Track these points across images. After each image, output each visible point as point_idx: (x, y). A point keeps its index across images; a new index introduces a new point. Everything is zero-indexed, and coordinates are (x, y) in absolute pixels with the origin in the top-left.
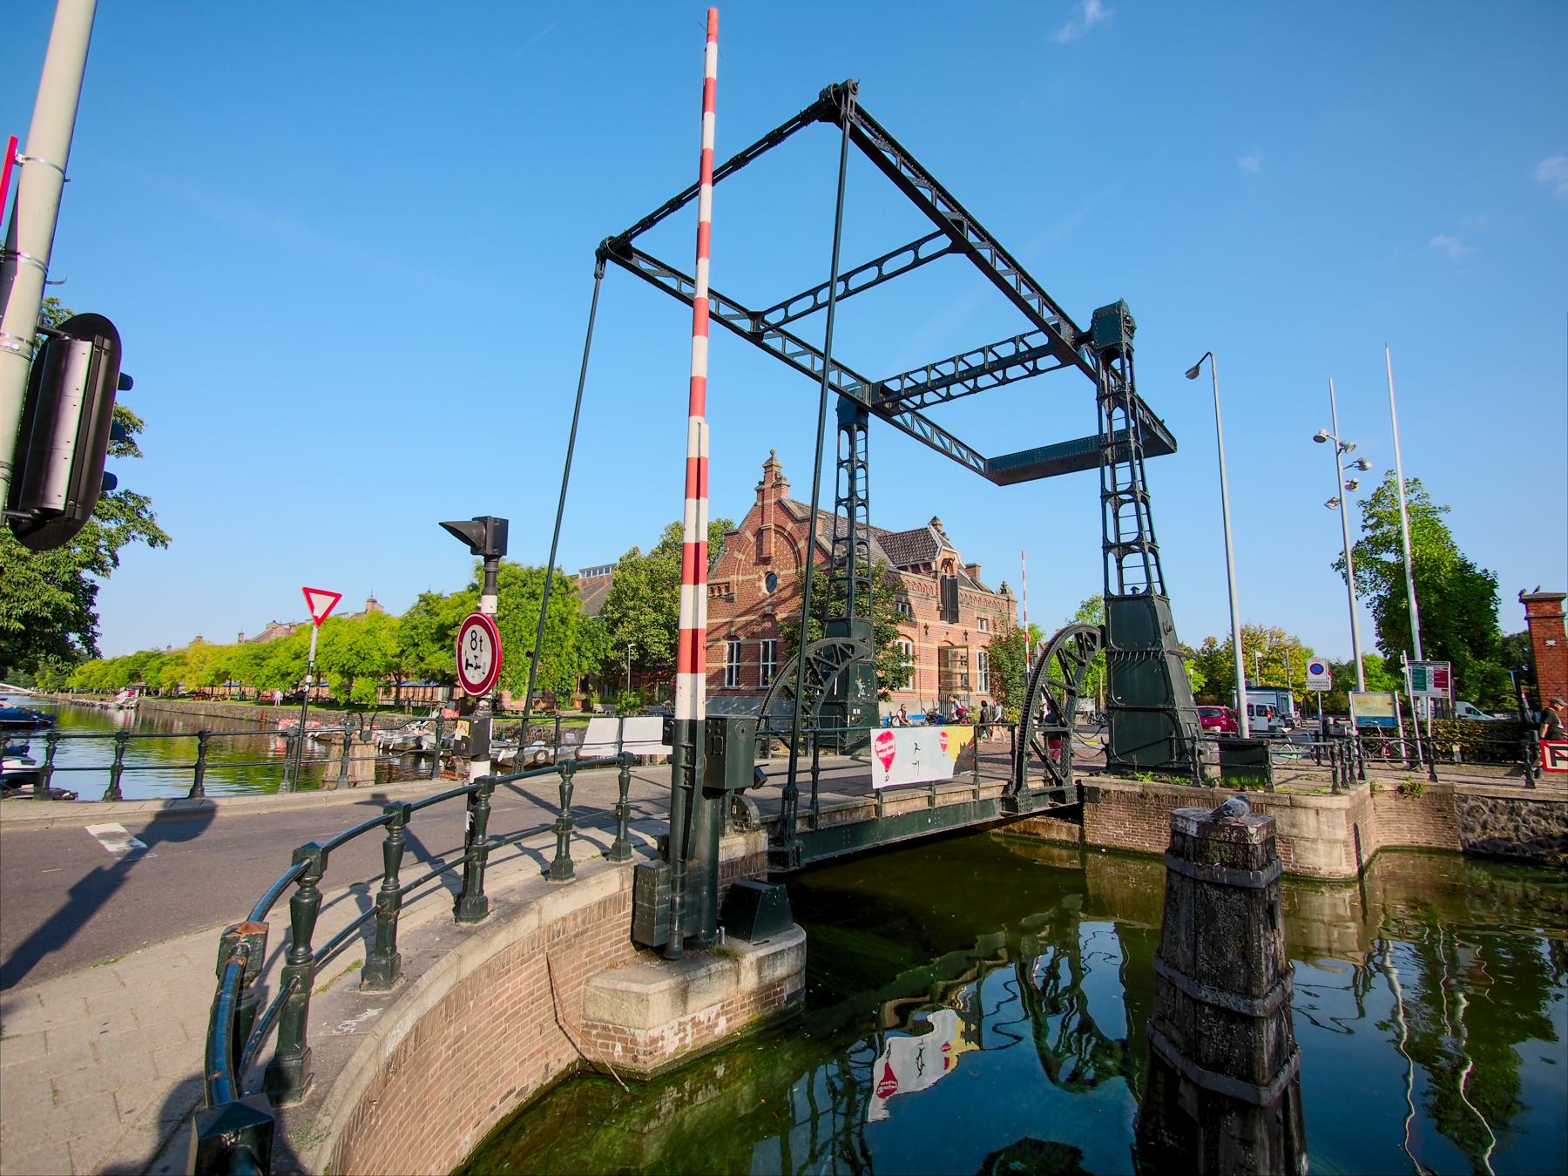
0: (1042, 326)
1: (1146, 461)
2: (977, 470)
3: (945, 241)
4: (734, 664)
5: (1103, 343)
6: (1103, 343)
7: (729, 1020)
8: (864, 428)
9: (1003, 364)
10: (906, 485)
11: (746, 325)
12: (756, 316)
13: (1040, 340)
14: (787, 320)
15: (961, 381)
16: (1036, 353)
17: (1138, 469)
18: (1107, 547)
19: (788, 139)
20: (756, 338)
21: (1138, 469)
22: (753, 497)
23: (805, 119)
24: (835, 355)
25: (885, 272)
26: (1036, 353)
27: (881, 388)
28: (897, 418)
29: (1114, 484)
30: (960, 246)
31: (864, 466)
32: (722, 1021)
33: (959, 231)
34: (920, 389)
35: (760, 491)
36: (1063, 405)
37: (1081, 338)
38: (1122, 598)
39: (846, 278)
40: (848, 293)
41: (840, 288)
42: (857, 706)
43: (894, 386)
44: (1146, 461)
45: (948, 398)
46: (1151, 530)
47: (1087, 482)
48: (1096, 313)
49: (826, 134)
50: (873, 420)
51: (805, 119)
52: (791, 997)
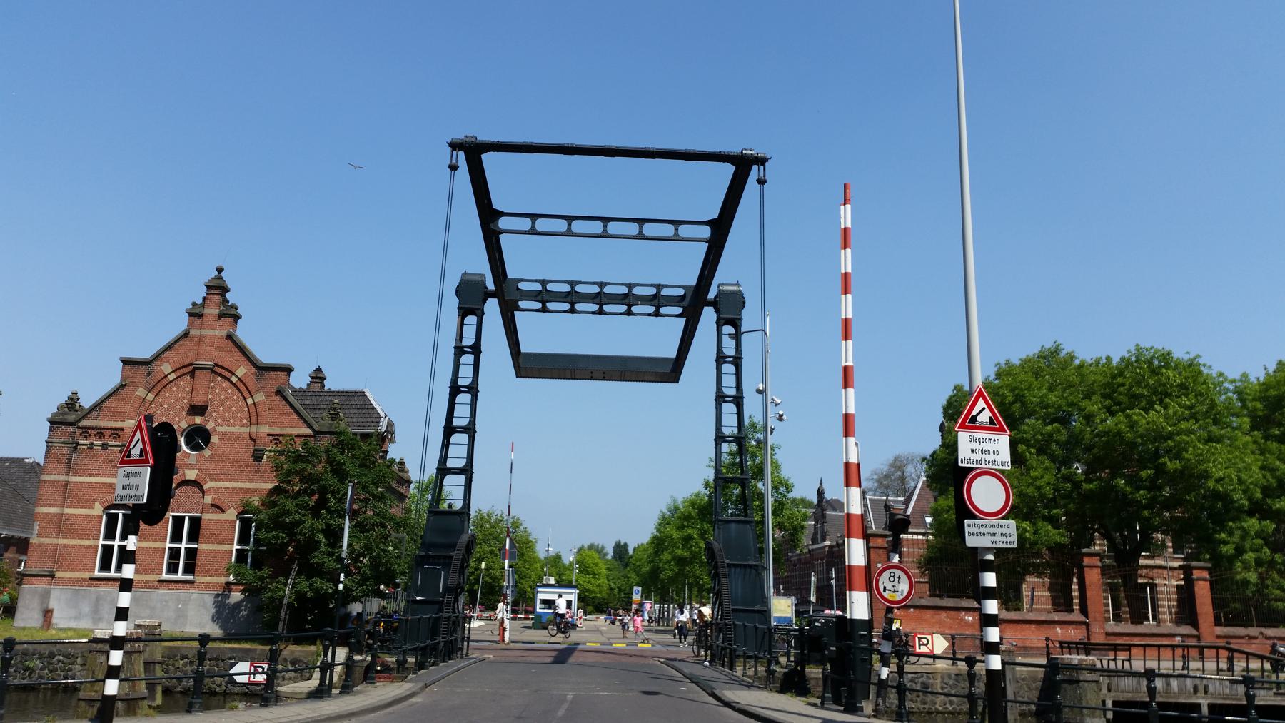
4: (184, 545)
22: (182, 323)
35: (195, 314)
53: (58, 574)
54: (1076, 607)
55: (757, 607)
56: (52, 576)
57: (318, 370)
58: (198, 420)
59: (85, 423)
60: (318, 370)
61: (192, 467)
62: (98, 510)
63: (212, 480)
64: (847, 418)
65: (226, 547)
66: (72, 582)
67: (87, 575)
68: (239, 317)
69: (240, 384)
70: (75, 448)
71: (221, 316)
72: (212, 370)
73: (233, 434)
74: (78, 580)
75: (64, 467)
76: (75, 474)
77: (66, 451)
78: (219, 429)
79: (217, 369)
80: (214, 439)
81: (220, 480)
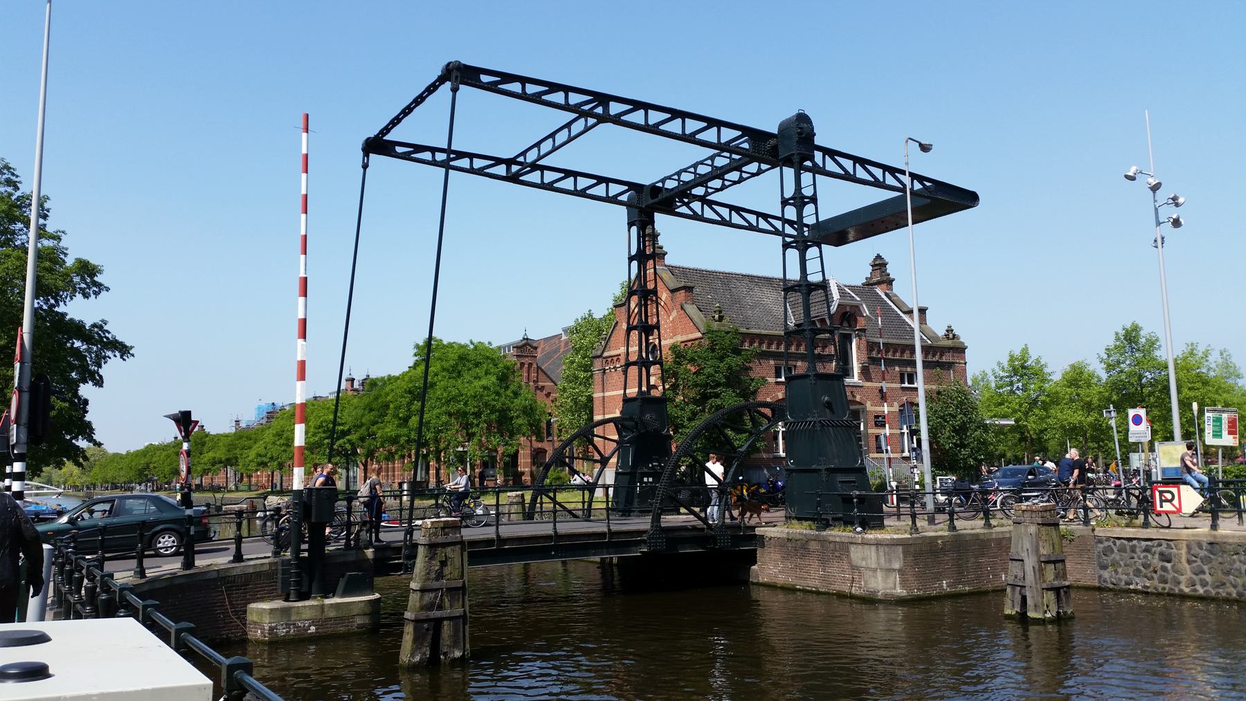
12: (509, 162)
14: (540, 158)
20: (514, 178)
27: (654, 190)
28: (684, 210)
32: (313, 629)
52: (359, 626)
57: (879, 257)
59: (606, 354)
60: (879, 257)
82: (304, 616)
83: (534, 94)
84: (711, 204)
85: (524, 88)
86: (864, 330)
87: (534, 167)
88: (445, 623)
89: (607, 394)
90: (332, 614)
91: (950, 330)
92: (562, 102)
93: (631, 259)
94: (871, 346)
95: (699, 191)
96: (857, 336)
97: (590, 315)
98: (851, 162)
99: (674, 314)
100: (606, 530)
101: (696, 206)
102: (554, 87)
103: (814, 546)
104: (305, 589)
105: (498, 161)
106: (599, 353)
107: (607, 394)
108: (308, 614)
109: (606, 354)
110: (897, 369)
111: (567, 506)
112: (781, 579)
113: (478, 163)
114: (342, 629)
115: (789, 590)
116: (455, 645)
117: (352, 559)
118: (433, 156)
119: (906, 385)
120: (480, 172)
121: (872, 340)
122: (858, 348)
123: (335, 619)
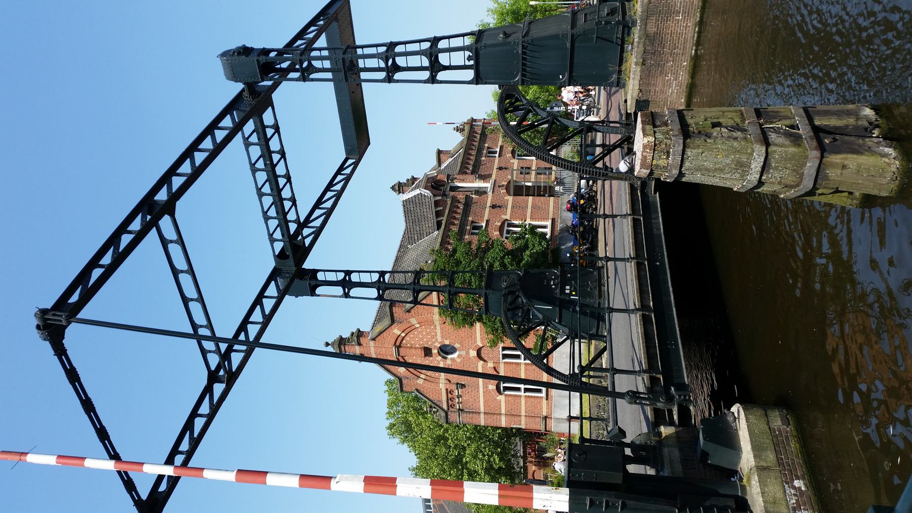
0: (237, 128)
1: (358, 43)
2: (356, 165)
3: (165, 222)
5: (257, 74)
6: (257, 74)
7: (798, 478)
8: (315, 272)
9: (267, 153)
10: (369, 233)
11: (162, 196)
12: (213, 377)
13: (249, 126)
15: (267, 140)
16: (261, 128)
17: (367, 51)
18: (433, 80)
19: (74, 365)
20: (232, 378)
21: (367, 51)
23: (60, 351)
24: (258, 351)
25: (174, 237)
26: (261, 128)
27: (281, 256)
28: (307, 242)
29: (379, 69)
30: (169, 208)
31: (348, 273)
32: (797, 483)
33: (153, 209)
34: (284, 223)
36: (305, 110)
37: (251, 87)
38: (476, 68)
39: (195, 326)
40: (210, 326)
41: (203, 332)
42: (563, 290)
43: (279, 246)
44: (358, 43)
45: (288, 178)
46: (420, 41)
47: (377, 97)
48: (228, 79)
49: (74, 335)
50: (308, 265)
51: (60, 351)
52: (786, 422)
53: (545, 414)
54: (789, 202)
55: (568, 45)
56: (546, 418)
57: (393, 188)
58: (435, 351)
59: (445, 407)
60: (393, 188)
61: (468, 353)
62: (502, 398)
63: (476, 342)
64: (324, 480)
65: (523, 367)
66: (549, 407)
67: (544, 401)
68: (359, 330)
69: (406, 331)
70: (462, 410)
71: (359, 344)
72: (399, 347)
73: (442, 333)
74: (548, 405)
75: (475, 416)
76: (479, 408)
77: (465, 415)
78: (439, 340)
79: (398, 344)
80: (447, 342)
81: (475, 338)
82: (779, 495)
83: (190, 443)
84: (308, 220)
85: (181, 453)
86: (448, 176)
87: (225, 357)
88: (817, 123)
89: (482, 410)
90: (771, 456)
91: (457, 129)
92: (204, 420)
93: (346, 295)
94: (463, 171)
95: (293, 227)
96: (452, 180)
97: (414, 469)
98: (318, 225)
99: (413, 321)
100: (630, 218)
101: (306, 232)
102: (189, 425)
103: (652, 29)
104: (731, 503)
105: (208, 390)
106: (443, 414)
107: (482, 410)
108: (775, 489)
109: (445, 407)
110: (483, 159)
111: (592, 355)
112: (684, 77)
113: (205, 409)
114: (794, 445)
115: (696, 61)
116: (856, 114)
117: (676, 453)
118: (181, 453)
119: (497, 155)
120: (215, 409)
121: (457, 171)
122: (463, 181)
123: (777, 453)
